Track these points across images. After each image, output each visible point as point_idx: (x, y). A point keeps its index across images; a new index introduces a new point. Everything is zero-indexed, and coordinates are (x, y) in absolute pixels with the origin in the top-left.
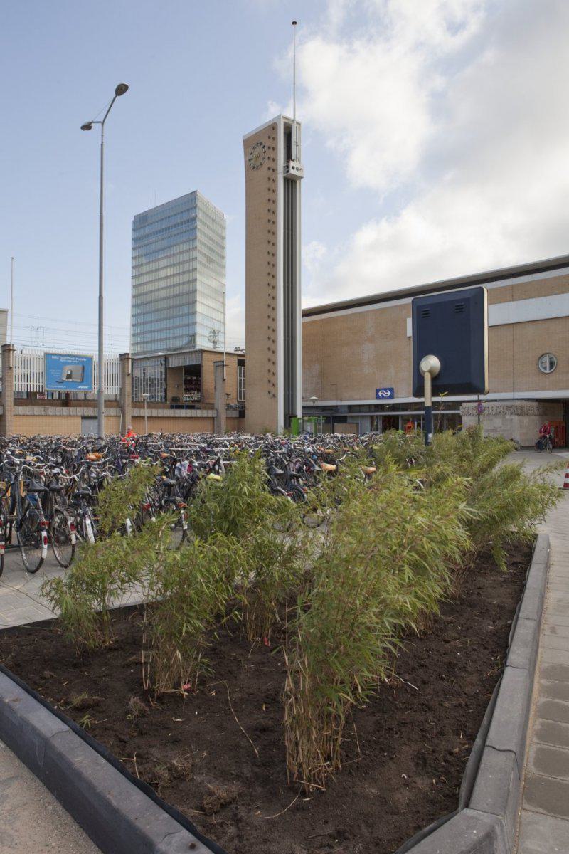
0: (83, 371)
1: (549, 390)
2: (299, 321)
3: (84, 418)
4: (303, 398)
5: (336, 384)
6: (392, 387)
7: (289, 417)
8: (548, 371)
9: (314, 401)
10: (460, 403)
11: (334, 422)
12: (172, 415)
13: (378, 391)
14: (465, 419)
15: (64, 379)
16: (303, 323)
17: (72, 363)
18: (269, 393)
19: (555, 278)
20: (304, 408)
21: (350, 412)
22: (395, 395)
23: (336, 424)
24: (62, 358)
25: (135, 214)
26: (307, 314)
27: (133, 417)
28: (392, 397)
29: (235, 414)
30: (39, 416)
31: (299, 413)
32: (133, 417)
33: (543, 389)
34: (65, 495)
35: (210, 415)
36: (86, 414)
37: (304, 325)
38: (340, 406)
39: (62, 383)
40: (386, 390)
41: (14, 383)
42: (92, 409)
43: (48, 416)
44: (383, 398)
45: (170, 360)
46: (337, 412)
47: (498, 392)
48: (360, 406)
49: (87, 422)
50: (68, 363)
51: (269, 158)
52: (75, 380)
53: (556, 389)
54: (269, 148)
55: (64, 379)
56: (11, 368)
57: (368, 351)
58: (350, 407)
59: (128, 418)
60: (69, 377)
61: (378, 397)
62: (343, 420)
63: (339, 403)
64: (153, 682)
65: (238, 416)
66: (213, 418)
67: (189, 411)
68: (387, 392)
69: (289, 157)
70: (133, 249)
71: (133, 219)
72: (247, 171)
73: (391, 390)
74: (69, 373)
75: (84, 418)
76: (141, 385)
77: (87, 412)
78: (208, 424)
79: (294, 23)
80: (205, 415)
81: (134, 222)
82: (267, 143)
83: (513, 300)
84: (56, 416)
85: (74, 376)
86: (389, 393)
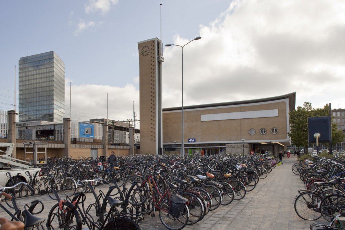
0: (91, 130)
1: (253, 140)
2: (162, 112)
3: (91, 149)
5: (170, 137)
7: (160, 149)
8: (274, 133)
10: (226, 144)
11: (170, 150)
13: (189, 139)
14: (227, 149)
15: (85, 133)
16: (163, 114)
17: (88, 127)
18: (152, 140)
19: (256, 106)
20: (163, 145)
22: (196, 141)
24: (84, 124)
25: (21, 57)
26: (164, 110)
27: (108, 149)
28: (195, 141)
29: (136, 148)
30: (75, 148)
31: (162, 147)
32: (108, 149)
33: (251, 140)
35: (129, 148)
36: (92, 148)
37: (164, 114)
39: (84, 135)
40: (192, 139)
41: (71, 134)
42: (94, 145)
43: (80, 148)
45: (56, 127)
46: (171, 147)
47: (235, 140)
49: (93, 150)
50: (87, 127)
51: (151, 53)
52: (89, 134)
53: (255, 140)
54: (151, 49)
55: (85, 133)
56: (70, 128)
57: (185, 125)
59: (107, 149)
60: (87, 132)
61: (189, 142)
62: (173, 149)
63: (172, 144)
66: (129, 149)
69: (158, 54)
70: (19, 73)
71: (19, 59)
72: (140, 56)
73: (195, 139)
74: (87, 131)
75: (91, 149)
76: (22, 135)
77: (93, 147)
78: (127, 151)
79: (161, 5)
81: (20, 61)
82: (151, 47)
83: (240, 111)
84: (78, 148)
85: (88, 132)
86: (190, 140)
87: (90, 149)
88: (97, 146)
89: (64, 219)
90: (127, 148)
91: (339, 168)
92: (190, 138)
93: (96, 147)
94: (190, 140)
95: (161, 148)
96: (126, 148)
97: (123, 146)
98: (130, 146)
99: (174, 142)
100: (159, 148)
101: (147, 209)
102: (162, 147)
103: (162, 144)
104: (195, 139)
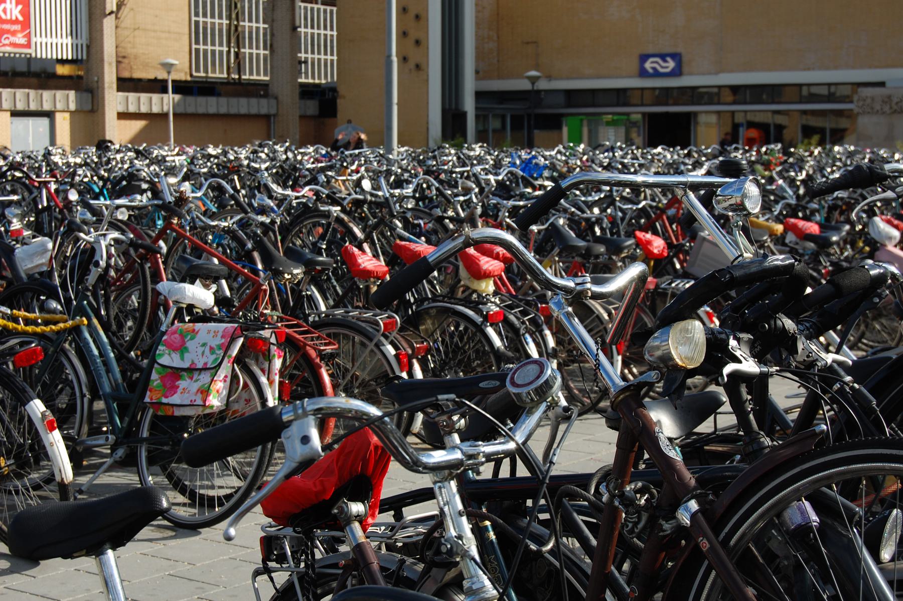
4: (477, 72)
6: (678, 50)
9: (533, 80)
12: (201, 110)
13: (644, 58)
20: (480, 95)
21: (569, 105)
22: (685, 69)
23: (536, 132)
28: (677, 72)
29: (312, 107)
31: (469, 105)
34: (788, 228)
35: (264, 111)
36: (20, 106)
38: (546, 91)
40: (663, 57)
43: (829, 85)
44: (657, 74)
48: (593, 92)
58: (569, 93)
61: (643, 73)
64: (768, 541)
65: (317, 112)
66: (267, 117)
67: (201, 100)
68: (665, 61)
73: (676, 56)
75: (15, 114)
80: (212, 110)
86: (648, 65)
87: (9, 114)
88: (47, 95)
89: (645, 312)
90: (254, 111)
91: (130, 360)
92: (651, 51)
93: (47, 99)
94: (648, 65)
95: (464, 115)
96: (243, 111)
97: (254, 101)
98: (276, 98)
99: (529, 78)
100: (444, 112)
101: (308, 348)
102: (469, 105)
103: (469, 85)
104: (676, 56)
